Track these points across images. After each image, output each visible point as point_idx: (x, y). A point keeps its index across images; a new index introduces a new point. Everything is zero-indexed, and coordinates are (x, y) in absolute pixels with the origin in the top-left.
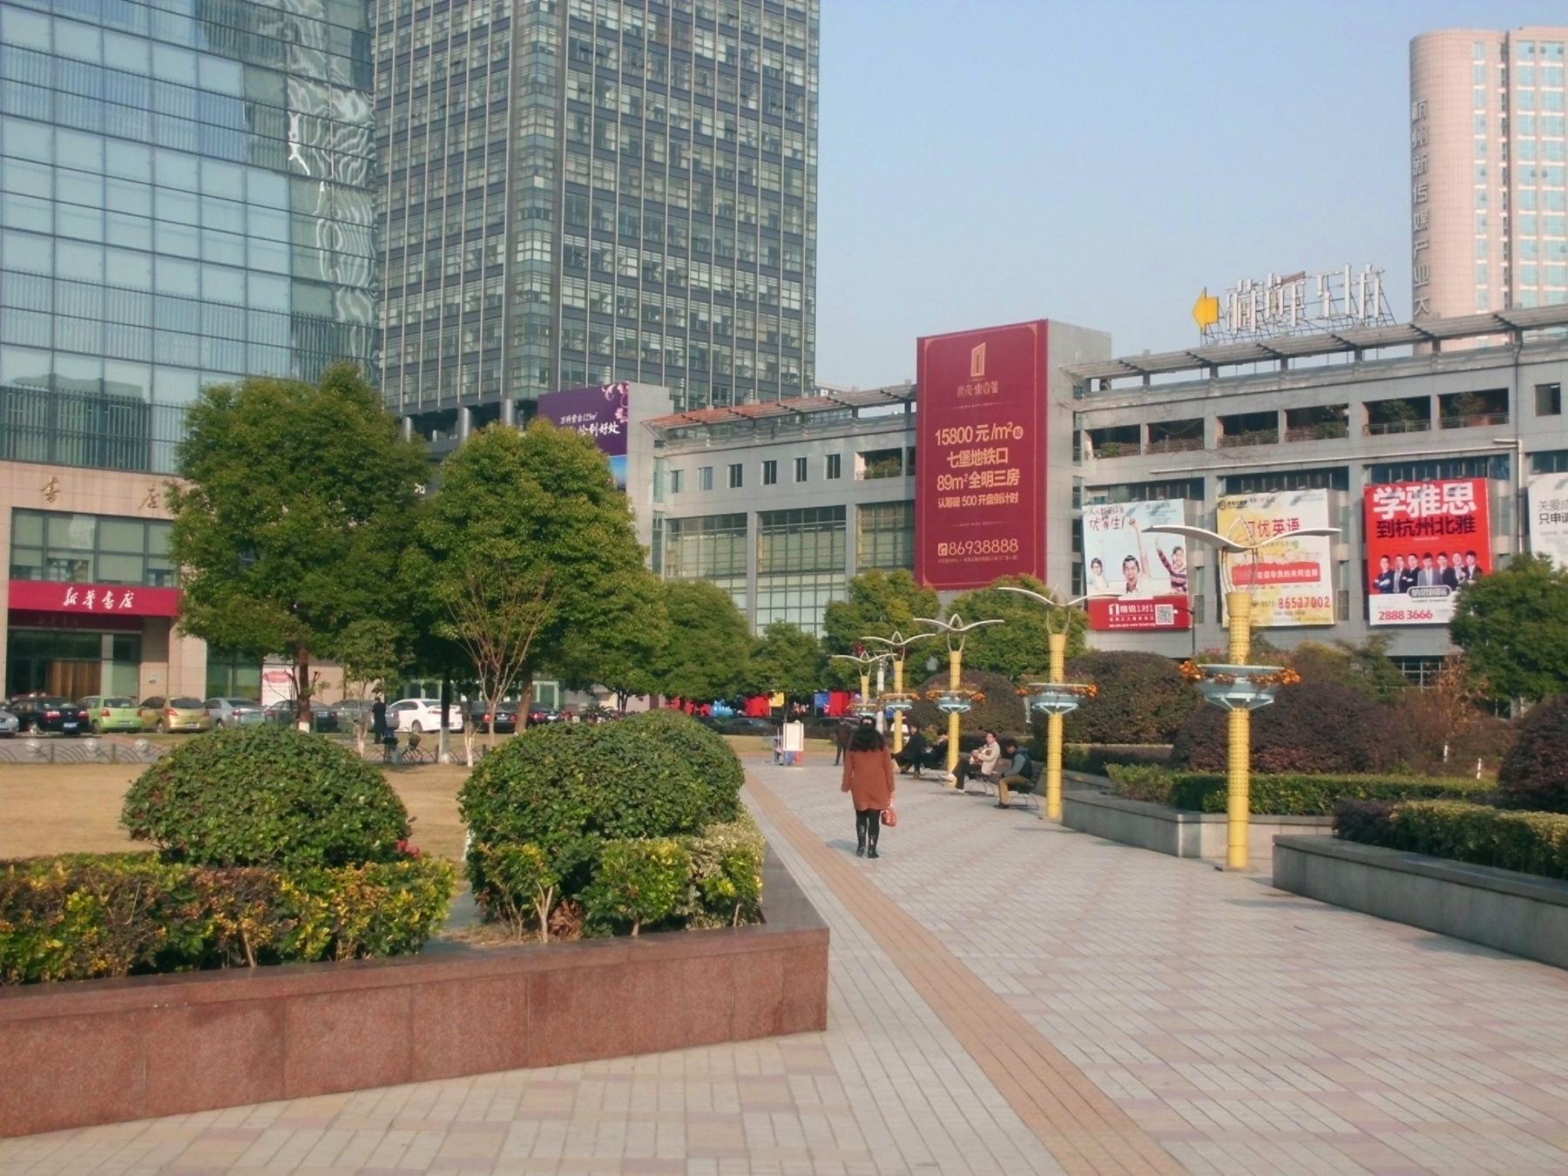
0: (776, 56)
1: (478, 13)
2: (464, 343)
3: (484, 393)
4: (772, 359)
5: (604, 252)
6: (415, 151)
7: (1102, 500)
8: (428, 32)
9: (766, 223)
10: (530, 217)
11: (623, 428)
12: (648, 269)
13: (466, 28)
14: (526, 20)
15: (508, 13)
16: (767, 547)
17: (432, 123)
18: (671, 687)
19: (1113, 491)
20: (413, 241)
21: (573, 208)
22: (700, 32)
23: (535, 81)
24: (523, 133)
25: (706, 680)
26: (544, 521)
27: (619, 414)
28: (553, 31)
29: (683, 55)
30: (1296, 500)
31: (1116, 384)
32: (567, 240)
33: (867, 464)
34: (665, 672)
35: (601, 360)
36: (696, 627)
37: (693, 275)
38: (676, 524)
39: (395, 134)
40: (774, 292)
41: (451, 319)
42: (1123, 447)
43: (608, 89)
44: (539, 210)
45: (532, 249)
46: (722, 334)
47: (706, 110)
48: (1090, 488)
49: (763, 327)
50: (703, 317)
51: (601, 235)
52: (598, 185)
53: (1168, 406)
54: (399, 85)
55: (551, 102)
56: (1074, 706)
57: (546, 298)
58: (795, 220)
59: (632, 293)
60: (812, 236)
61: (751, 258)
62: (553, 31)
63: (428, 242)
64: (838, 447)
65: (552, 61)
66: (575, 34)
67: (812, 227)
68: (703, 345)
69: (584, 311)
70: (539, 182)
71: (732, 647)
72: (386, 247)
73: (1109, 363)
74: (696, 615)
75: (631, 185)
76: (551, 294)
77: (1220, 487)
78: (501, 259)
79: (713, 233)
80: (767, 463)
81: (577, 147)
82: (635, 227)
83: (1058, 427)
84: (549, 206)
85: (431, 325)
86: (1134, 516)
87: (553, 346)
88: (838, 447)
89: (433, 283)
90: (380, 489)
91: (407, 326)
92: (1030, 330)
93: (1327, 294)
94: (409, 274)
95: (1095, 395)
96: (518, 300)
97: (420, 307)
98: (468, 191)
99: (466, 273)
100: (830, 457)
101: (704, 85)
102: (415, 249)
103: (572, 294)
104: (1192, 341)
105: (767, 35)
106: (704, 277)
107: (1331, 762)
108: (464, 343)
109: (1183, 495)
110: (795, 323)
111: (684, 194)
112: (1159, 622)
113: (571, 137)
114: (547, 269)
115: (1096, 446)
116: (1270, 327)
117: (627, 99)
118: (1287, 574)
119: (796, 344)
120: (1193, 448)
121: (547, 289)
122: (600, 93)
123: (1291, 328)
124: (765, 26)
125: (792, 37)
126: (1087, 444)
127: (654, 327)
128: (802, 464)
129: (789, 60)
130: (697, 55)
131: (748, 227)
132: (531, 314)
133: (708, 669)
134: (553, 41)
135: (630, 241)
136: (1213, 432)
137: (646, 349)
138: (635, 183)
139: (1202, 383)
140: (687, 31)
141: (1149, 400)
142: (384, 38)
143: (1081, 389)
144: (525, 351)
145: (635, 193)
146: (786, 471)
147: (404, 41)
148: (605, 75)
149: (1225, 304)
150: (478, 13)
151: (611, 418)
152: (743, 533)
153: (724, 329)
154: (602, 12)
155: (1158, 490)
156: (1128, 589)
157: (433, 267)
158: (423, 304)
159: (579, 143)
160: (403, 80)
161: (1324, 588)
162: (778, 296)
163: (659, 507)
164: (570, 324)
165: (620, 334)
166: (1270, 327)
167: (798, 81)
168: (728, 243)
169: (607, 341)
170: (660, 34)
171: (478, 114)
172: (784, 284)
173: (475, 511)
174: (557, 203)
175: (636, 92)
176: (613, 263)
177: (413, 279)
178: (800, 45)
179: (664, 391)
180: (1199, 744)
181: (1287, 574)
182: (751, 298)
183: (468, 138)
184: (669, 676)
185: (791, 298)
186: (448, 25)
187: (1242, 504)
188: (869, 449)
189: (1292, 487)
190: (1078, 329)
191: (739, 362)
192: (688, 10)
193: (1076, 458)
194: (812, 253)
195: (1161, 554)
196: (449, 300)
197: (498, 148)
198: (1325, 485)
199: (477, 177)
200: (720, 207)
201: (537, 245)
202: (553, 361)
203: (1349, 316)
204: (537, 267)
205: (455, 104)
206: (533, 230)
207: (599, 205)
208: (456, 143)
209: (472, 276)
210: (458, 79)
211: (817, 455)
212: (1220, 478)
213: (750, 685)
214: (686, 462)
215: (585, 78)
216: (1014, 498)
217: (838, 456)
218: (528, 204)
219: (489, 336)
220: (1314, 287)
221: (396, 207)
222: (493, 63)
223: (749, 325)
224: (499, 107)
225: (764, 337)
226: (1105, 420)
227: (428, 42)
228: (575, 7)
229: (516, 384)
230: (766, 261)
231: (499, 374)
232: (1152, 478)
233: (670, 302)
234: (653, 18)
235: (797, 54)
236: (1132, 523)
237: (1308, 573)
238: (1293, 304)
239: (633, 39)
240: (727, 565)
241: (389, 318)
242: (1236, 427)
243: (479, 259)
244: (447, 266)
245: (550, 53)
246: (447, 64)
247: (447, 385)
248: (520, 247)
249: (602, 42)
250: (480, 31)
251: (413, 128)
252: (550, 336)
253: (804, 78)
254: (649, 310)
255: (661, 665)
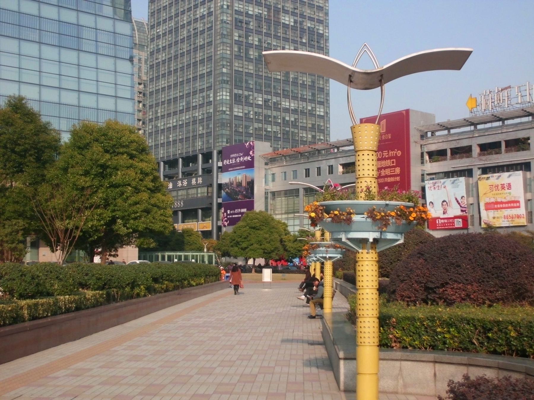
0: (313, 23)
1: (202, 10)
2: (199, 130)
3: (206, 148)
4: (314, 134)
5: (249, 95)
6: (181, 62)
7: (433, 179)
8: (185, 18)
9: (310, 84)
10: (222, 83)
11: (253, 158)
12: (266, 101)
13: (198, 16)
14: (219, 12)
15: (212, 10)
16: (307, 202)
17: (187, 51)
18: (248, 254)
19: (437, 175)
20: (181, 94)
21: (237, 80)
22: (284, 14)
23: (222, 34)
24: (219, 53)
25: (262, 251)
26: (104, 167)
27: (251, 153)
28: (229, 15)
29: (277, 23)
30: (510, 176)
31: (437, 134)
32: (236, 91)
33: (343, 168)
34: (246, 248)
35: (249, 135)
36: (258, 229)
37: (283, 103)
38: (273, 193)
39: (174, 56)
40: (314, 109)
41: (194, 122)
42: (440, 158)
43: (250, 36)
44: (225, 80)
45: (223, 95)
46: (294, 125)
47: (287, 43)
48: (428, 174)
49: (310, 122)
50: (287, 118)
51: (248, 89)
52: (247, 71)
53: (458, 141)
54: (175, 38)
55: (229, 41)
56: (339, 256)
57: (228, 113)
58: (321, 82)
59: (260, 110)
60: (328, 88)
61: (305, 97)
62: (229, 15)
63: (186, 94)
64: (332, 162)
65: (229, 26)
66: (237, 16)
67: (327, 85)
68: (287, 129)
69: (242, 117)
70: (224, 70)
71: (273, 237)
72: (172, 97)
73: (434, 125)
74: (258, 225)
75: (259, 71)
76: (230, 111)
77: (479, 172)
78: (212, 99)
79: (290, 88)
80: (306, 169)
81: (238, 57)
82: (261, 86)
83: (415, 151)
84: (228, 79)
85: (188, 124)
86: (445, 184)
87: (231, 130)
88: (332, 162)
89: (188, 109)
90: (31, 155)
91: (179, 125)
92: (403, 114)
93: (520, 94)
94: (180, 106)
95: (429, 138)
96: (218, 114)
97: (184, 118)
98: (200, 75)
99: (199, 105)
100: (329, 166)
101: (286, 34)
102: (182, 97)
103: (238, 111)
104: (467, 115)
105: (309, 15)
106: (287, 104)
107: (498, 294)
108: (199, 130)
109: (465, 176)
110: (322, 120)
111: (279, 74)
112: (456, 226)
113: (236, 54)
114: (228, 102)
115: (430, 158)
116: (497, 108)
117: (257, 39)
118: (507, 205)
119: (322, 128)
120: (468, 157)
121: (228, 109)
122: (247, 37)
123: (506, 108)
124: (308, 12)
125: (318, 16)
126: (427, 157)
127: (270, 123)
128: (319, 169)
129: (318, 24)
130: (283, 23)
131: (303, 85)
132: (222, 119)
133: (263, 247)
134: (229, 19)
135: (259, 91)
136: (476, 150)
137: (266, 131)
138: (261, 70)
139: (471, 131)
140: (279, 14)
141: (450, 139)
142: (170, 22)
143: (423, 136)
144: (220, 132)
145: (260, 74)
146: (313, 172)
147: (177, 23)
148: (248, 31)
149: (479, 100)
150: (202, 10)
151: (248, 155)
152: (298, 196)
153: (296, 123)
154: (247, 8)
155: (455, 174)
156: (444, 213)
157: (188, 103)
158: (184, 117)
159: (240, 56)
160: (177, 36)
161: (522, 211)
162: (315, 110)
163: (267, 188)
164: (237, 122)
165: (256, 125)
166: (497, 108)
167: (321, 32)
168: (296, 91)
169: (251, 128)
170: (269, 16)
171: (202, 47)
172: (318, 106)
173: (71, 162)
174: (231, 78)
175: (260, 37)
176: (253, 100)
177: (181, 108)
178: (322, 19)
179: (268, 144)
180: (402, 281)
181: (507, 205)
182: (305, 111)
183: (199, 56)
184: (247, 250)
185: (320, 111)
186: (192, 15)
187: (488, 178)
188: (344, 162)
189: (508, 171)
190: (422, 112)
191: (301, 135)
192: (279, 6)
193: (422, 163)
194: (328, 94)
195: (456, 199)
196: (194, 115)
197: (210, 59)
198: (521, 169)
199: (203, 70)
200: (293, 78)
201: (224, 93)
202: (231, 136)
203: (529, 102)
204: (224, 101)
205: (194, 44)
206: (222, 88)
207: (247, 78)
208: (195, 58)
209: (202, 106)
210: (196, 35)
211: (324, 166)
212: (479, 168)
213: (292, 253)
214: (276, 170)
215: (241, 32)
216: (398, 179)
217: (332, 166)
218: (221, 78)
219: (208, 127)
220: (514, 92)
221: (175, 82)
222: (207, 28)
223: (305, 121)
224: (210, 44)
225: (310, 126)
226: (433, 148)
227: (185, 22)
228: (237, 6)
229: (218, 145)
230: (310, 98)
231: (211, 141)
232: (452, 170)
233: (275, 113)
234: (266, 10)
235: (320, 22)
236: (445, 187)
237: (515, 205)
238: (506, 98)
239: (258, 18)
240: (292, 208)
241: (173, 123)
242: (485, 148)
243: (204, 99)
244: (193, 102)
245: (228, 23)
246: (192, 30)
247: (194, 146)
248: (218, 94)
249: (247, 19)
250: (203, 17)
251: (180, 54)
252: (230, 126)
253: (323, 30)
254: (267, 116)
255: (244, 245)
